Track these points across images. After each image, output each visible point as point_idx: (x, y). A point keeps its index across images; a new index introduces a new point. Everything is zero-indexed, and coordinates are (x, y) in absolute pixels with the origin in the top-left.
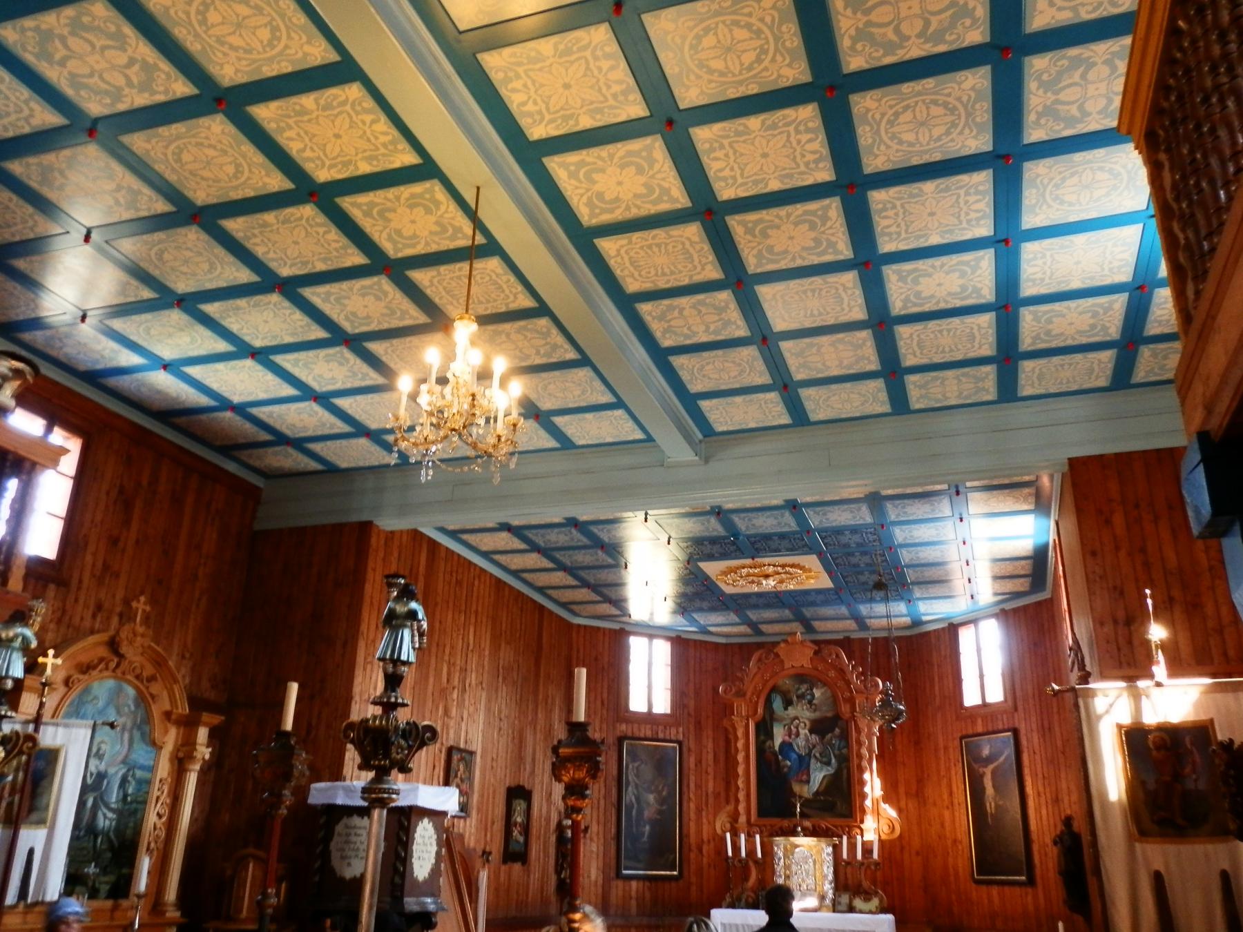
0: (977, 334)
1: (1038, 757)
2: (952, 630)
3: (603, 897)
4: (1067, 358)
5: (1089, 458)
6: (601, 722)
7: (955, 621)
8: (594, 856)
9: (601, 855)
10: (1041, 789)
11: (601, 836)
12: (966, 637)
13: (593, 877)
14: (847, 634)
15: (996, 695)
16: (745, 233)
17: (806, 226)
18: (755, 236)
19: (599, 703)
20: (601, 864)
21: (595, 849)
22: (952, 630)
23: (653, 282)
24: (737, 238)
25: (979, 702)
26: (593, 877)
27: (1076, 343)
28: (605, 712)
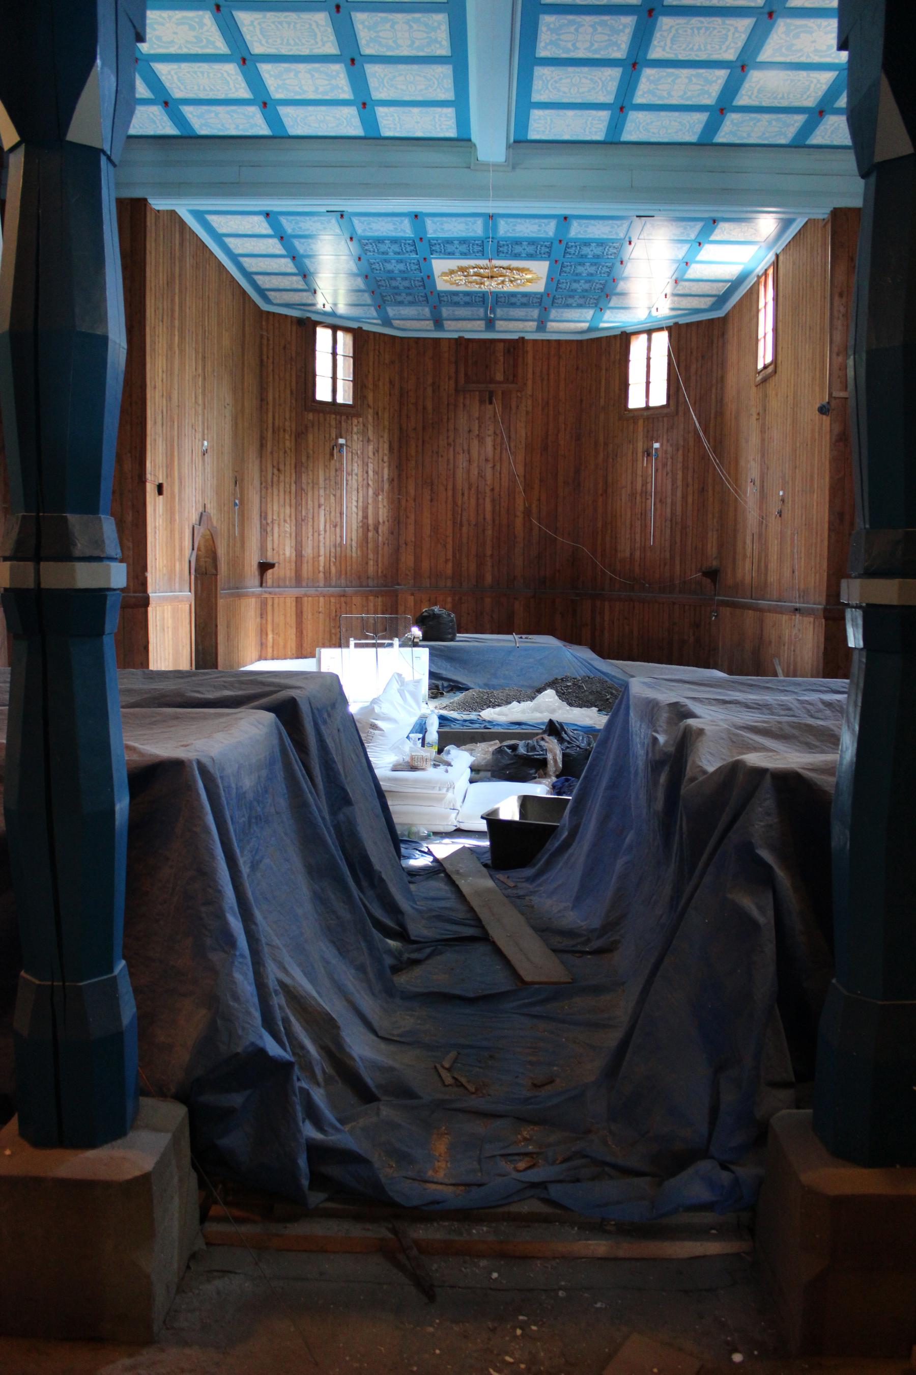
0: (669, 42)
1: (691, 455)
2: (624, 339)
3: (296, 571)
4: (693, 57)
5: (849, 209)
6: (291, 411)
7: (629, 329)
8: (288, 535)
9: (294, 535)
10: (690, 480)
11: (293, 518)
12: (638, 347)
13: (288, 553)
14: (522, 335)
15: (659, 398)
16: (214, 42)
17: (186, 28)
18: (207, 39)
19: (288, 391)
20: (293, 544)
21: (288, 530)
22: (624, 339)
23: (675, 54)
24: (222, 39)
25: (643, 405)
26: (288, 553)
27: (809, 61)
28: (294, 401)
